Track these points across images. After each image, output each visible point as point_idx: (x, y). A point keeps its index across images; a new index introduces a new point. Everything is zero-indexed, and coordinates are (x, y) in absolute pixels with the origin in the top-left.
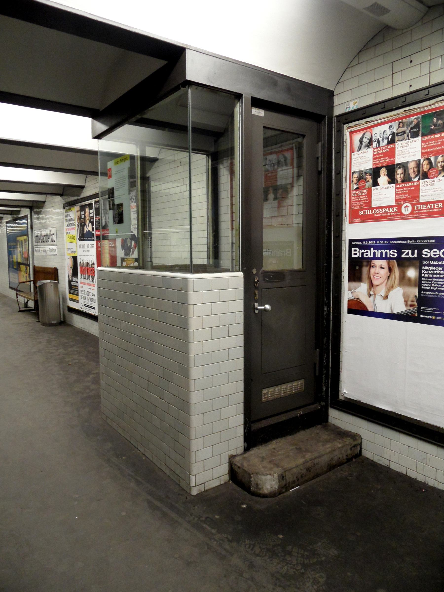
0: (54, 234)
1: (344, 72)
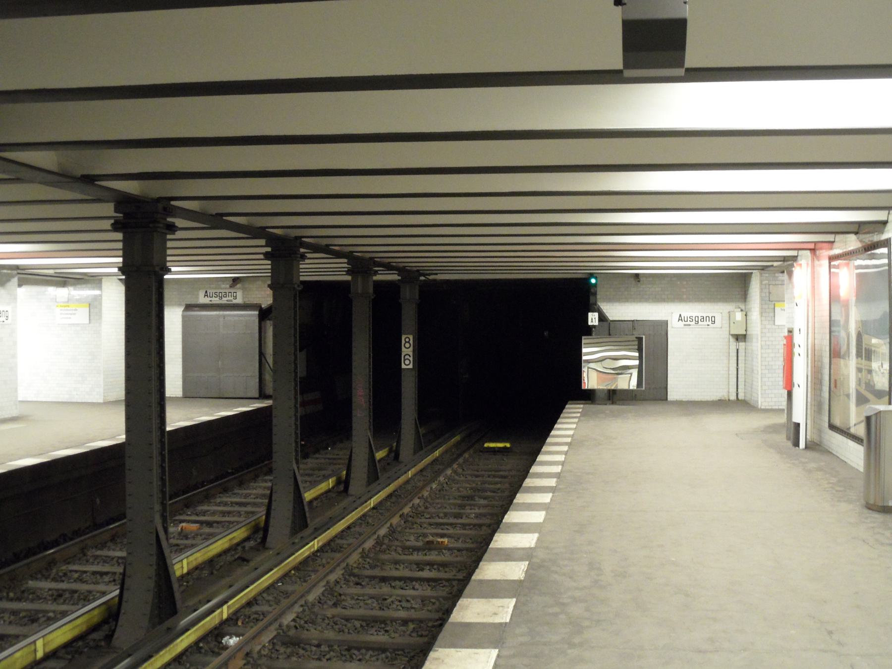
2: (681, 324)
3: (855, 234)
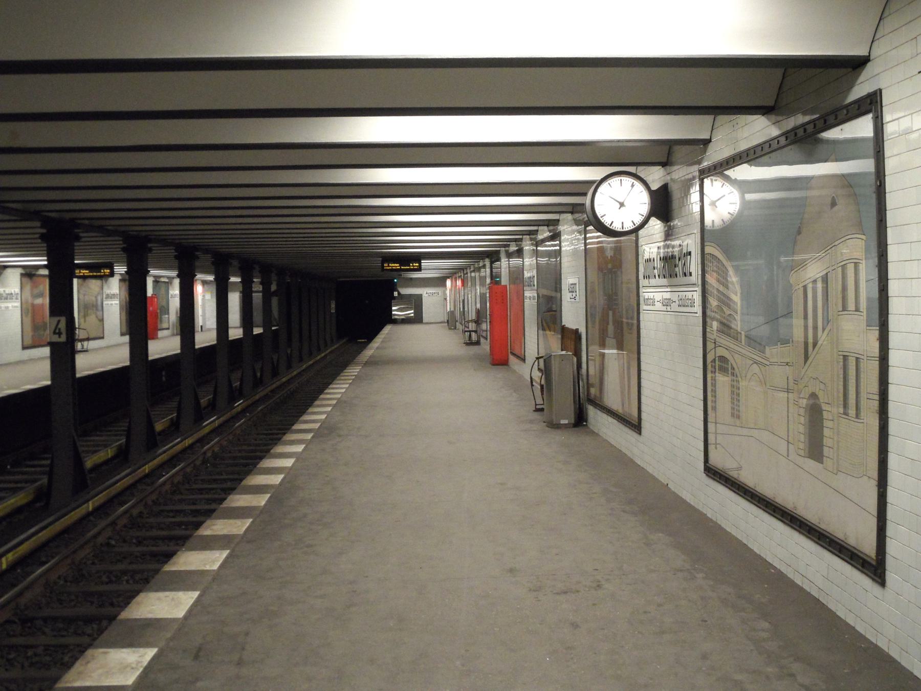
0: (690, 253)
1: (876, 29)
2: (427, 295)
3: (663, 167)
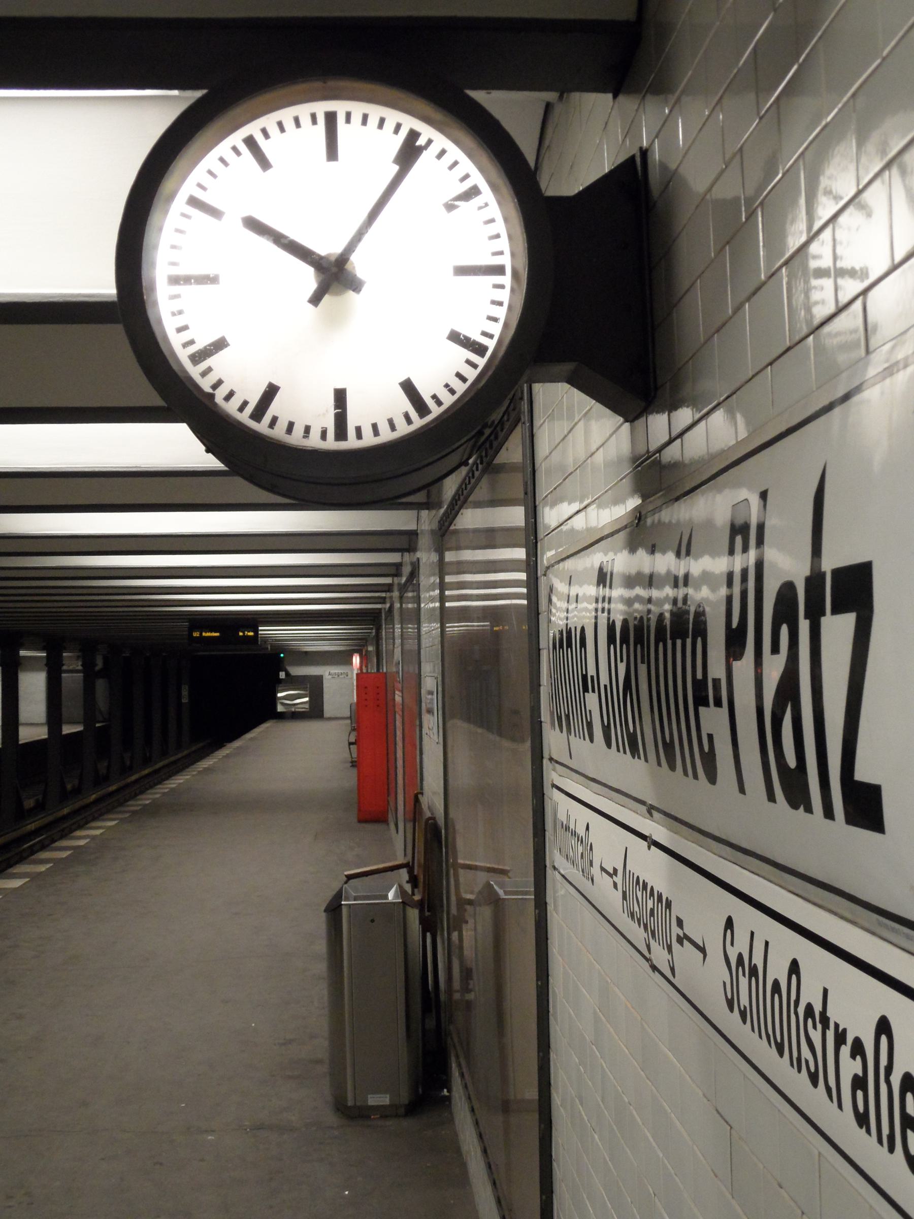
2: (330, 677)
